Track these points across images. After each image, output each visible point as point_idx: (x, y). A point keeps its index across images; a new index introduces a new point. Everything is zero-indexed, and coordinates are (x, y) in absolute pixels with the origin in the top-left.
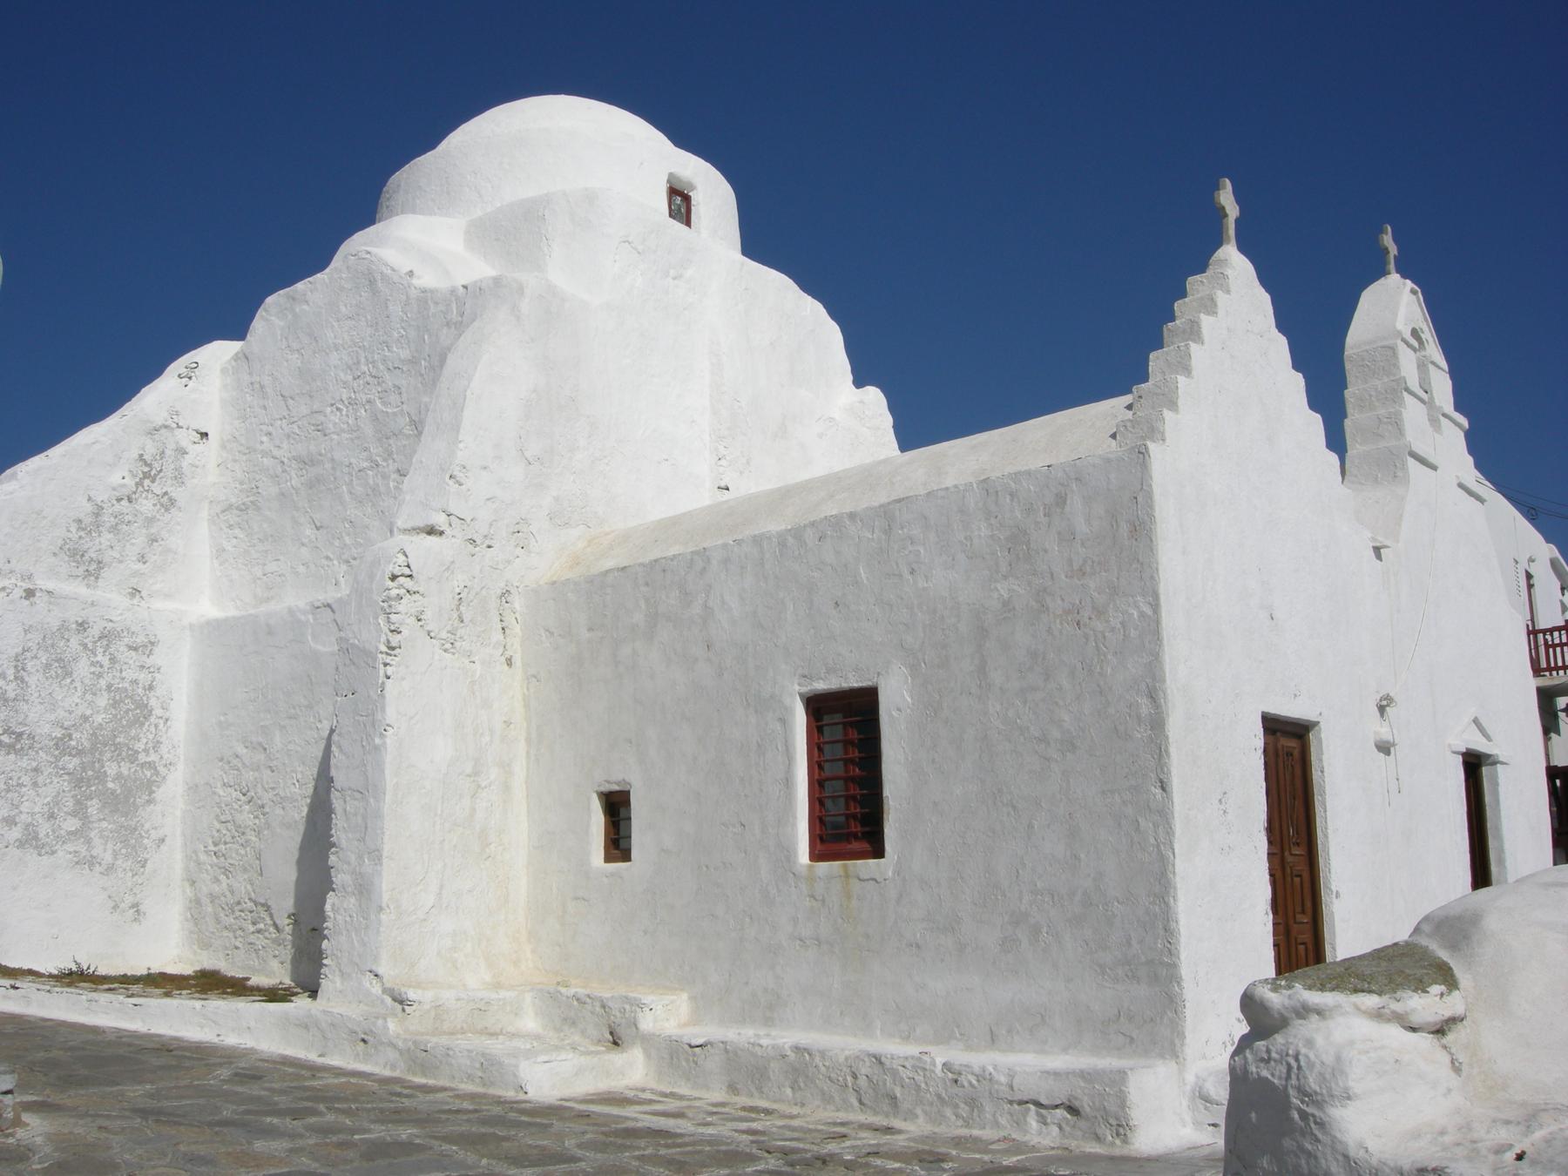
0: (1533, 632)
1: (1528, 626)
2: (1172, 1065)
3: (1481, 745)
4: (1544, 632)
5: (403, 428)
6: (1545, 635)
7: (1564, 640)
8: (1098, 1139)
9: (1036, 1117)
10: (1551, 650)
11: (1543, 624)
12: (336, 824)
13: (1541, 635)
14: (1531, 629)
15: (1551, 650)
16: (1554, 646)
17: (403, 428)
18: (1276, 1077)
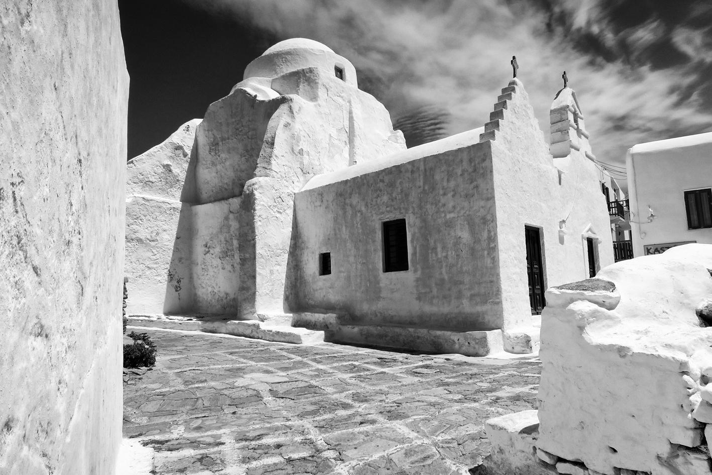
3: (592, 236)
5: (615, 214)
16: (612, 208)
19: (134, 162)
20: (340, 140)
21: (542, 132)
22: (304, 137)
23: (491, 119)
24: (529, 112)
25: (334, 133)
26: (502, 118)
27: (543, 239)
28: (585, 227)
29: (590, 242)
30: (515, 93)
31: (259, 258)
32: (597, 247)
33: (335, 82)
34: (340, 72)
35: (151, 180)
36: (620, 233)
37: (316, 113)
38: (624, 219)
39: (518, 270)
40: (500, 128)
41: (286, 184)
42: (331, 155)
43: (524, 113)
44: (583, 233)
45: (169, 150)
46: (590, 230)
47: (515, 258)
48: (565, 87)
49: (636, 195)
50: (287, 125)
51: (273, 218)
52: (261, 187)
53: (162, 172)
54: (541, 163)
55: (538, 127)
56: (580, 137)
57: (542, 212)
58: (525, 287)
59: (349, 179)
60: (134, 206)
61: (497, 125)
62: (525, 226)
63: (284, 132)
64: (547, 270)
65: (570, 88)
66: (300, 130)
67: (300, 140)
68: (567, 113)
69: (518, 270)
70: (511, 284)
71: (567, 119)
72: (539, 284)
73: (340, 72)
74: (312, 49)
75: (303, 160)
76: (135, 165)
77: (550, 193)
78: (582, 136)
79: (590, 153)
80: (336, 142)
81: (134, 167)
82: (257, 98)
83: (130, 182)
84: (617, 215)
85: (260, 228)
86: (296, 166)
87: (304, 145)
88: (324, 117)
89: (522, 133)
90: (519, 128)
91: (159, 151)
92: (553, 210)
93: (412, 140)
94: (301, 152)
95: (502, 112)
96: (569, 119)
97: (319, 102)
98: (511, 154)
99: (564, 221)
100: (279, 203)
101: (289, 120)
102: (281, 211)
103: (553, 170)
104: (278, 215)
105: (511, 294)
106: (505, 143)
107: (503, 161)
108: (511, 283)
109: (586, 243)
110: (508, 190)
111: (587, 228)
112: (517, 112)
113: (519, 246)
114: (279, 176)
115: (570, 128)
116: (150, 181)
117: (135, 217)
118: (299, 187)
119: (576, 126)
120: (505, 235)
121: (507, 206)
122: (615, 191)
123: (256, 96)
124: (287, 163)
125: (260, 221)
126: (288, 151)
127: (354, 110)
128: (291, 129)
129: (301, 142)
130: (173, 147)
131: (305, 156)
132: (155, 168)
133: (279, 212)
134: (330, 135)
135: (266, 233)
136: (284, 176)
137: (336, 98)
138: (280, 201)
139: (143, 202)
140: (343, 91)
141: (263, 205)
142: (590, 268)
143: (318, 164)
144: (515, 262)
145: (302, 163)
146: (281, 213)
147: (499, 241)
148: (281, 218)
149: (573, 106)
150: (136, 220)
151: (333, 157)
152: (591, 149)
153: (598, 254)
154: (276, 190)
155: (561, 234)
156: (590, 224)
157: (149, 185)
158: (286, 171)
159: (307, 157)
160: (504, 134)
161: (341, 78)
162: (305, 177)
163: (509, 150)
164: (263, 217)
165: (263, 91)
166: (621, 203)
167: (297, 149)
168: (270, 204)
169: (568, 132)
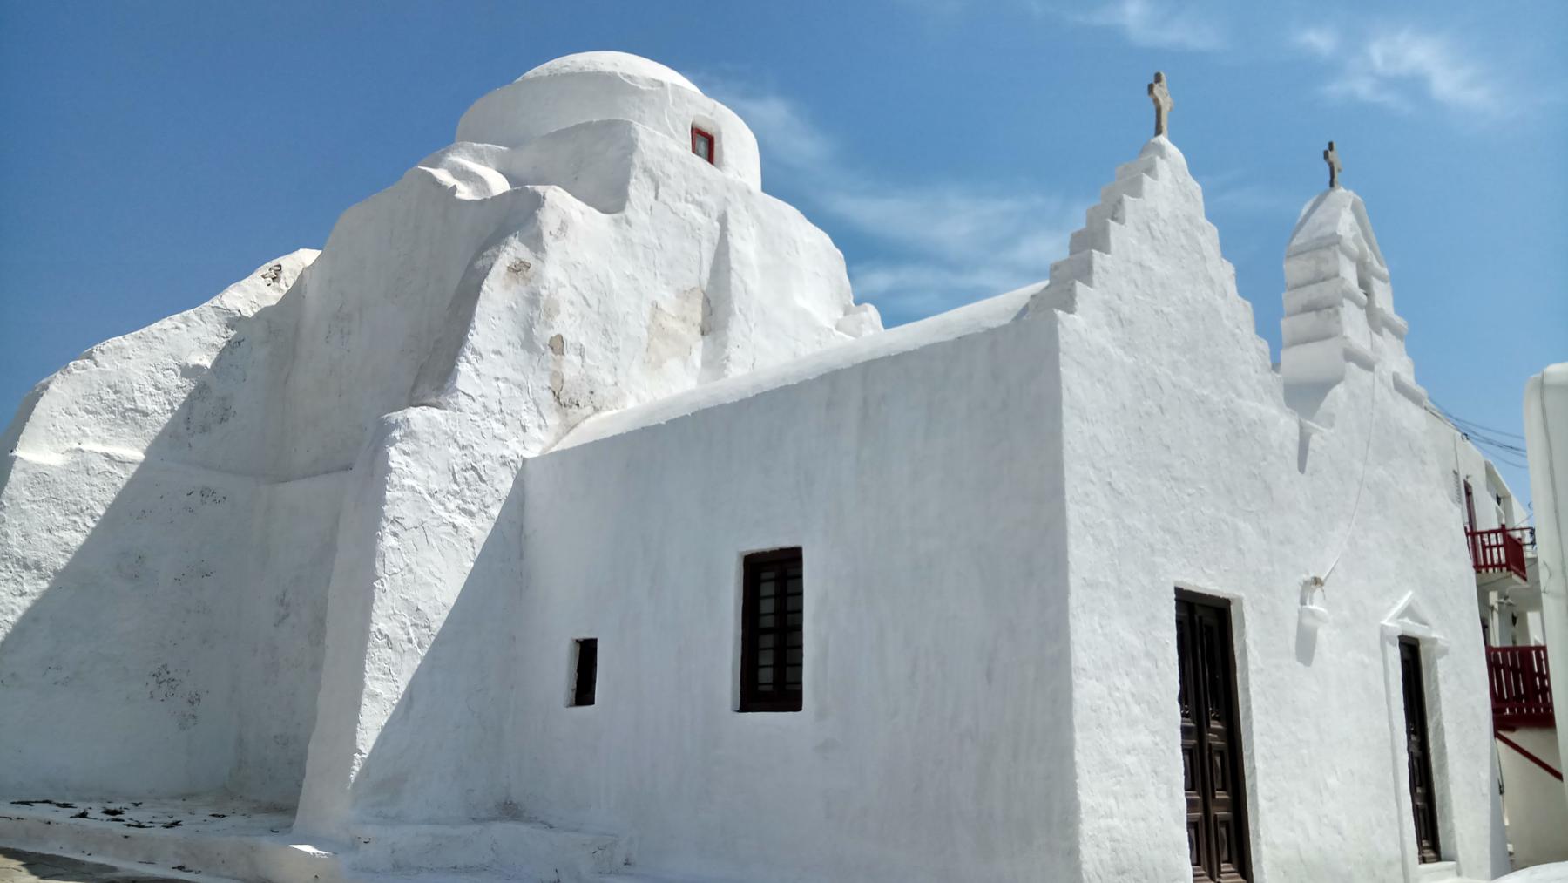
0: (1472, 533)
1: (1466, 529)
2: (738, 709)
3: (1415, 630)
4: (1481, 533)
5: (1500, 565)
6: (1482, 537)
7: (1500, 542)
8: (429, 420)
9: (541, 298)
10: (1488, 551)
11: (1480, 527)
12: (381, 600)
13: (1479, 537)
14: (1468, 530)
15: (1488, 551)
16: (1491, 547)
17: (1500, 565)
18: (102, 412)
19: (97, 355)
20: (684, 320)
21: (1248, 303)
22: (572, 303)
23: (1072, 253)
24: (1202, 239)
25: (667, 298)
26: (1105, 248)
27: (1242, 634)
28: (1395, 603)
29: (1411, 650)
30: (1155, 177)
31: (377, 646)
32: (1432, 665)
33: (683, 164)
34: (706, 143)
35: (140, 405)
36: (1514, 620)
37: (616, 241)
38: (1525, 579)
39: (1145, 739)
40: (1095, 278)
41: (498, 429)
42: (653, 360)
43: (1184, 241)
44: (1385, 622)
45: (209, 327)
46: (1409, 612)
47: (1133, 695)
48: (1332, 184)
49: (1556, 511)
50: (519, 269)
51: (443, 528)
52: (411, 435)
53: (177, 387)
54: (1239, 395)
55: (1232, 288)
56: (1379, 332)
57: (1240, 550)
58: (1171, 795)
59: (663, 423)
60: (74, 476)
61: (1085, 272)
62: (1178, 591)
63: (507, 287)
64: (1256, 739)
65: (1347, 188)
66: (559, 285)
67: (558, 312)
68: (1336, 256)
69: (1145, 739)
70: (1118, 788)
71: (1337, 275)
72: (1229, 786)
73: (706, 143)
74: (629, 77)
75: (560, 367)
76: (96, 364)
77: (1268, 488)
78: (1385, 331)
79: (1409, 378)
80: (674, 325)
81: (94, 368)
82: (458, 195)
83: (75, 408)
84: (1504, 569)
85: (391, 557)
86: (540, 384)
87: (566, 324)
88: (640, 254)
89: (1174, 298)
90: (1162, 285)
91: (177, 328)
92: (1281, 543)
93: (890, 321)
94: (557, 345)
95: (1105, 231)
96: (1342, 275)
97: (628, 212)
98: (1129, 361)
99: (1317, 581)
100: (469, 485)
101: (525, 253)
102: (474, 508)
103: (1282, 421)
104: (461, 520)
105: (1116, 822)
106: (1110, 325)
107: (1099, 381)
108: (1119, 782)
109: (1395, 655)
110: (1114, 473)
111: (1402, 604)
112: (1157, 234)
113: (1148, 655)
114: (478, 407)
115: (1345, 301)
116: (136, 410)
117: (73, 508)
118: (541, 442)
119: (1365, 297)
120: (1096, 618)
121: (1110, 522)
122: (1498, 500)
123: (454, 189)
124: (509, 373)
125: (395, 534)
126: (514, 339)
127: (735, 241)
128: (530, 280)
129: (558, 319)
130: (223, 319)
131: (571, 357)
132: (160, 376)
133: (464, 511)
134: (655, 306)
135: (411, 571)
136: (496, 408)
137: (680, 206)
138: (471, 480)
139: (107, 467)
140: (704, 189)
141: (412, 489)
142: (1409, 733)
143: (610, 380)
144: (1136, 710)
145: (557, 376)
146: (471, 514)
147: (1073, 638)
148: (471, 529)
149: (1355, 239)
150: (76, 518)
151: (658, 365)
152: (1411, 368)
153: (1437, 688)
154: (463, 447)
155: (1308, 621)
156: (1410, 593)
157: (133, 419)
158: (505, 394)
159: (577, 360)
160: (1107, 297)
161: (710, 158)
162: (567, 415)
163: (1123, 348)
164: (407, 523)
165: (481, 177)
166: (1517, 535)
167: (543, 335)
168: (434, 487)
169: (1337, 313)
